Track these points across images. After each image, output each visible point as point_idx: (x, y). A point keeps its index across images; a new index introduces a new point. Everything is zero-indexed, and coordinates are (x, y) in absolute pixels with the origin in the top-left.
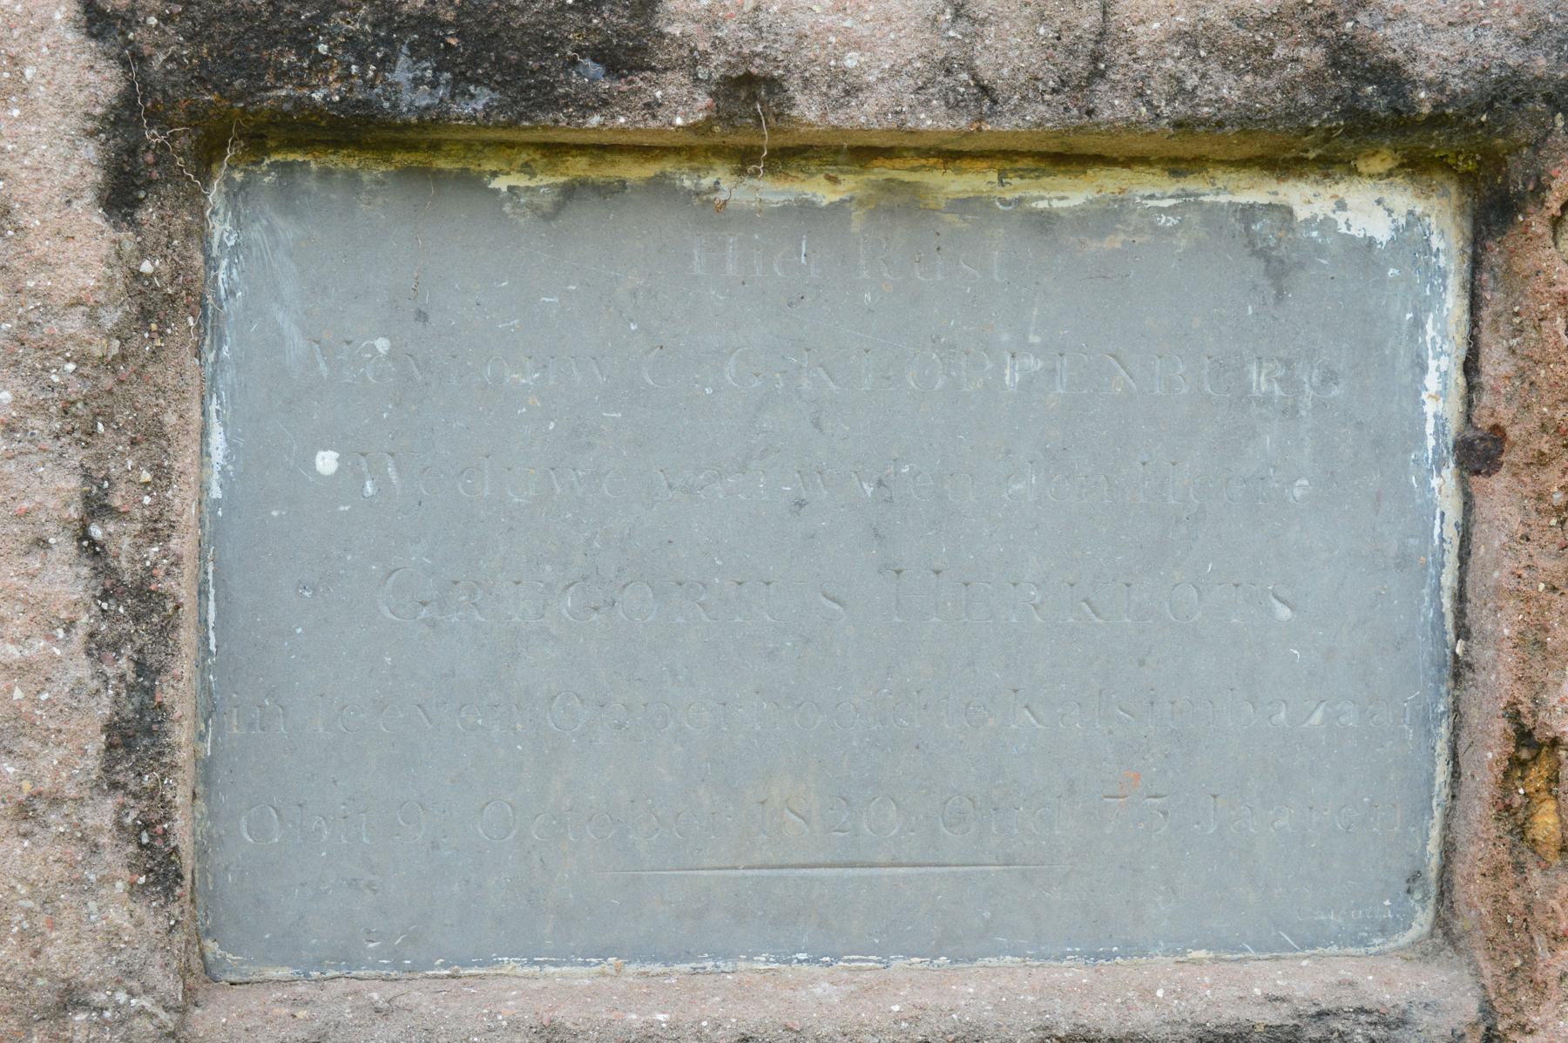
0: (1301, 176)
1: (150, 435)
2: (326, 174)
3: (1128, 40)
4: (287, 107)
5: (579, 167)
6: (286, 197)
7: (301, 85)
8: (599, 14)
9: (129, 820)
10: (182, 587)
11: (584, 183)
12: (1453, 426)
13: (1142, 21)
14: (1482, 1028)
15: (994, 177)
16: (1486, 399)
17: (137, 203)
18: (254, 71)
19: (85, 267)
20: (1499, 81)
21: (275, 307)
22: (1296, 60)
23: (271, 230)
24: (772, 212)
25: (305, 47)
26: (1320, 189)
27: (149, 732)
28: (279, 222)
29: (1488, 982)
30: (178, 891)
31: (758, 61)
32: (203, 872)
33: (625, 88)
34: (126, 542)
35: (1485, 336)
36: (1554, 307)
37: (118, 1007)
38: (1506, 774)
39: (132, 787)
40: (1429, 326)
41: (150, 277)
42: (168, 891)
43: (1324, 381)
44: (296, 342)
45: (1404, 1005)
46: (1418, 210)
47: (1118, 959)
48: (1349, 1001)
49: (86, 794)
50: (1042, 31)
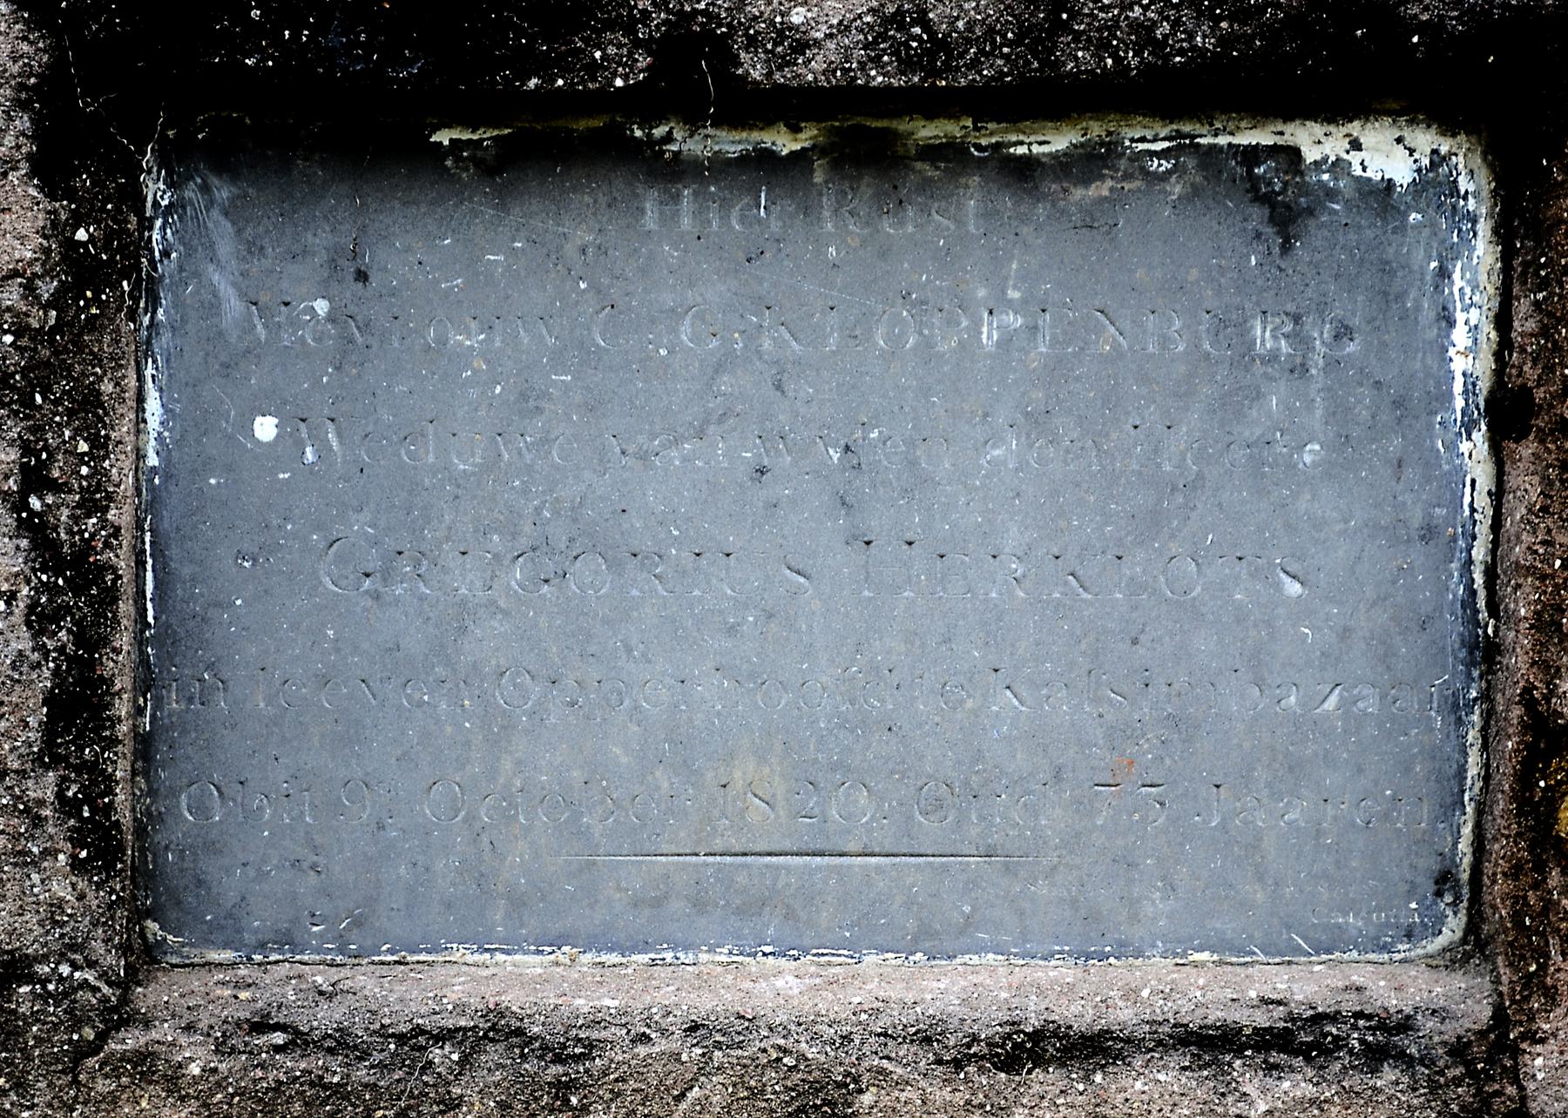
1: (89, 409)
9: (70, 794)
12: (1484, 386)
19: (22, 239)
21: (211, 268)
23: (205, 189)
26: (1332, 128)
28: (214, 181)
29: (1504, 989)
34: (65, 514)
37: (61, 979)
40: (1457, 276)
42: (109, 867)
44: (233, 305)
45: (1408, 1010)
46: (1444, 150)
47: (1112, 960)
48: (1350, 1004)
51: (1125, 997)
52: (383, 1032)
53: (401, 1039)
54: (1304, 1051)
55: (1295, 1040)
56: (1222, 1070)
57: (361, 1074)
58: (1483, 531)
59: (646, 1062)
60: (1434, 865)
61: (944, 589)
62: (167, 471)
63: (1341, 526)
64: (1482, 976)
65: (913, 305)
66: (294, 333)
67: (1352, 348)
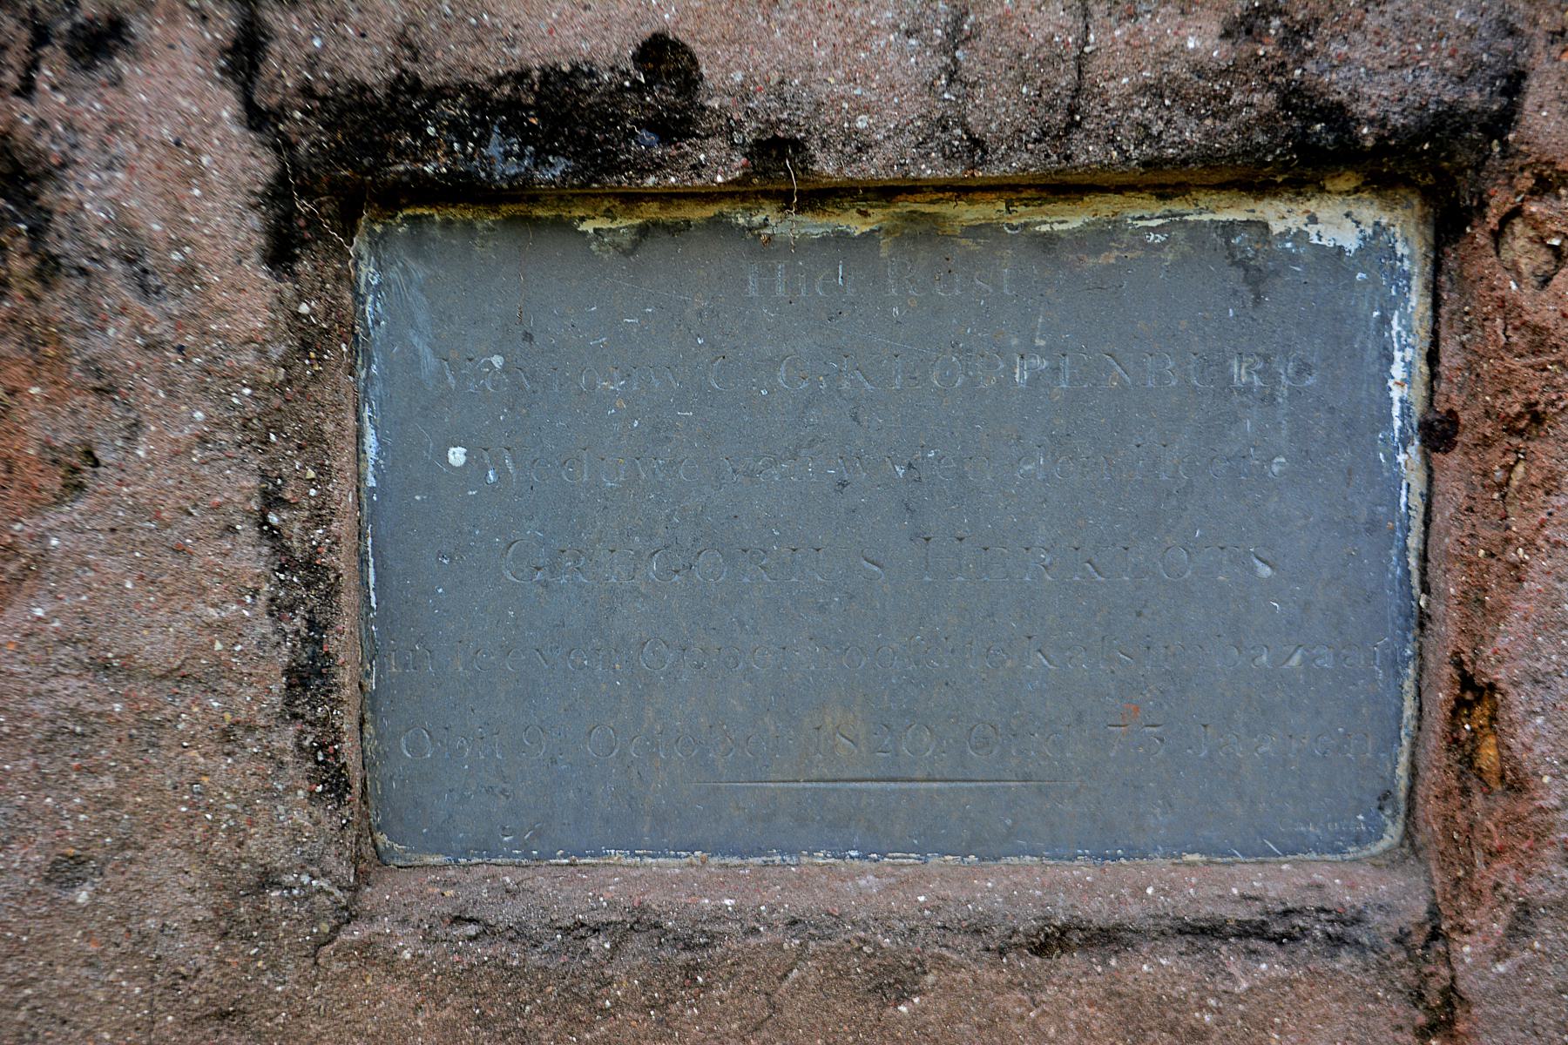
0: (1276, 195)
1: (313, 441)
2: (447, 224)
3: (1100, 94)
4: (405, 178)
5: (651, 211)
6: (417, 244)
7: (417, 160)
8: (651, 93)
9: (307, 743)
10: (342, 561)
11: (655, 224)
12: (1417, 410)
13: (1112, 77)
14: (1428, 928)
15: (1003, 206)
16: (1443, 387)
17: (296, 259)
18: (379, 150)
19: (254, 312)
20: (1437, 115)
21: (411, 332)
22: (1251, 105)
23: (405, 271)
24: (812, 242)
25: (418, 131)
26: (1293, 206)
27: (320, 675)
28: (412, 264)
29: (1437, 888)
30: (348, 797)
31: (783, 126)
32: (373, 780)
33: (675, 153)
34: (297, 526)
35: (1443, 332)
36: (1494, 310)
37: (302, 887)
38: (1454, 712)
39: (308, 717)
40: (1395, 323)
41: (307, 317)
42: (340, 797)
43: (1298, 373)
44: (429, 360)
45: (1360, 905)
46: (1384, 221)
47: (1123, 861)
48: (1313, 902)
49: (273, 723)
50: (1024, 90)
51: (1134, 896)
52: (553, 926)
53: (566, 931)
54: (1277, 939)
56: (1213, 956)
57: (535, 958)
58: (1417, 524)
59: (756, 950)
60: (1379, 788)
61: (988, 575)
62: (381, 489)
63: (1302, 522)
64: (1417, 875)
65: (960, 352)
66: (477, 383)
67: (1310, 381)
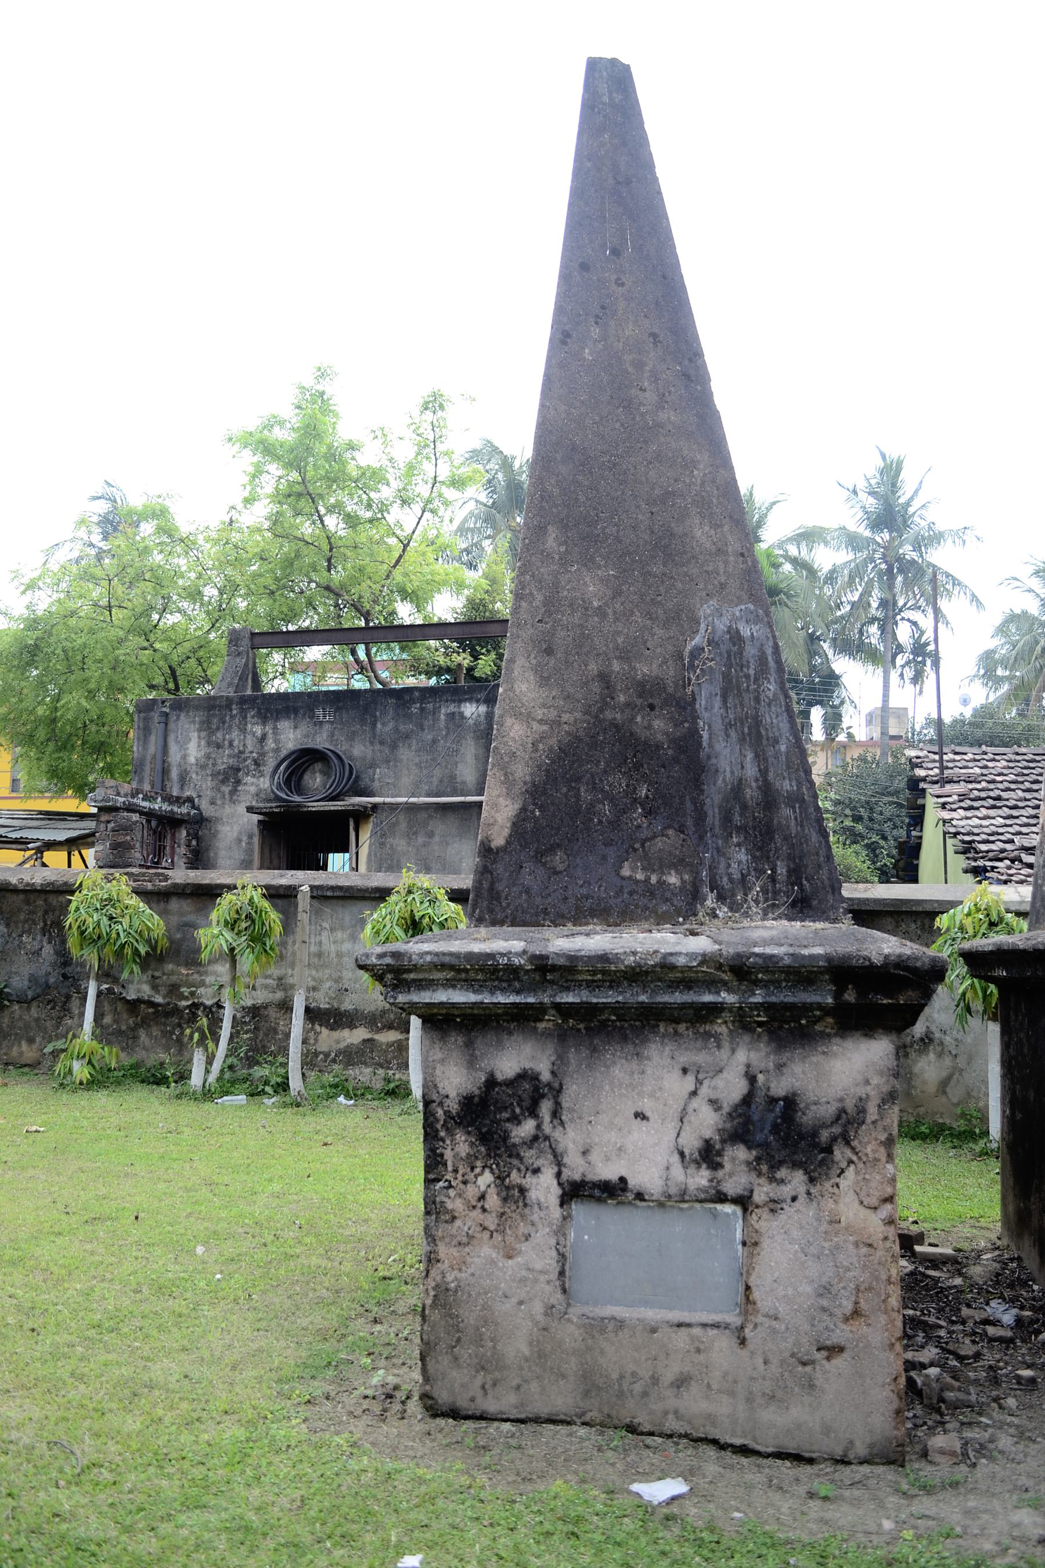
1: (564, 1235)
55: (716, 1326)
